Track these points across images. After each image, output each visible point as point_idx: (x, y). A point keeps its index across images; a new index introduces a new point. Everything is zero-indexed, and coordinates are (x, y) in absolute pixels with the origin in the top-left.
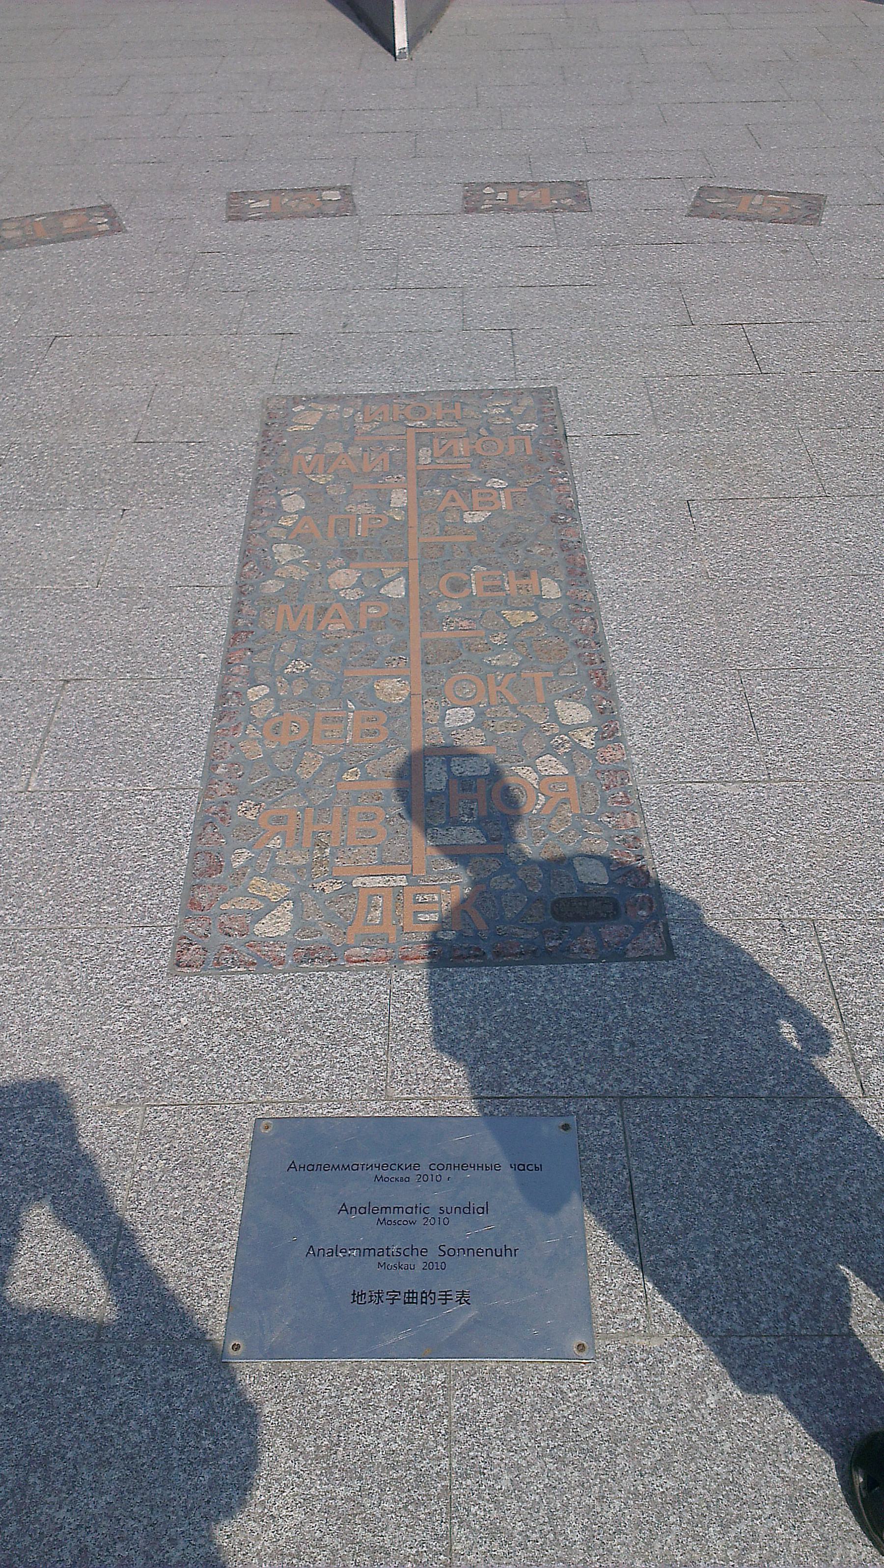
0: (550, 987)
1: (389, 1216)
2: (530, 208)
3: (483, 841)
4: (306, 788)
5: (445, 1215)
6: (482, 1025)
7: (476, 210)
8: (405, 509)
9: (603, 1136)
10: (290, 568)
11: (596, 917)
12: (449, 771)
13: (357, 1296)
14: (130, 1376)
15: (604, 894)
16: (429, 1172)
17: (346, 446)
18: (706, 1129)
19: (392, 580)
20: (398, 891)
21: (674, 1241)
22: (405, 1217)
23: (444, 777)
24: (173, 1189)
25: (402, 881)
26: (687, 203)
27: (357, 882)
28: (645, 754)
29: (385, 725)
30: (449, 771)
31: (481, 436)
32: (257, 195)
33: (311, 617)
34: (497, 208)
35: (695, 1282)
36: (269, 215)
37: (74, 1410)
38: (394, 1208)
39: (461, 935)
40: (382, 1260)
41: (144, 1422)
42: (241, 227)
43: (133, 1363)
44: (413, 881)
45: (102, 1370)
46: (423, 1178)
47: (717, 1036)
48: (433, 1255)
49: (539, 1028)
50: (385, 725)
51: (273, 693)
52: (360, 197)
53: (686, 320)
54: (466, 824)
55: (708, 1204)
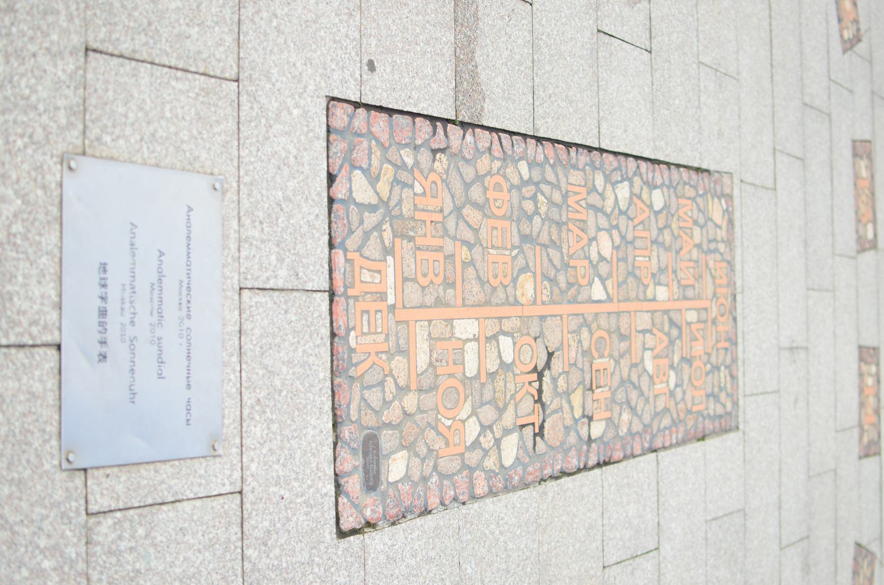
0: (317, 431)
1: (156, 292)
2: (862, 405)
3: (419, 371)
4: (458, 210)
5: (157, 342)
6: (291, 372)
7: (861, 359)
8: (654, 299)
9: (216, 476)
10: (612, 198)
11: (366, 471)
12: (468, 340)
13: (104, 268)
14: (64, 77)
15: (383, 478)
16: (185, 328)
17: (698, 246)
18: (221, 564)
19: (605, 288)
20: (383, 297)
21: (147, 536)
22: (156, 307)
23: (464, 337)
24: (183, 108)
25: (391, 300)
26: (864, 542)
27: (390, 259)
28: (480, 515)
29: (501, 283)
30: (468, 340)
31: (705, 365)
32: (871, 168)
33: (577, 216)
34: (861, 375)
35: (121, 552)
36: (857, 176)
37: (42, 32)
38: (377, 311)
39: (352, 350)
40: (128, 287)
41: (34, 91)
42: (848, 153)
43: (71, 78)
44: (392, 308)
45: (67, 54)
46: (181, 320)
47: (285, 575)
48: (130, 331)
49: (289, 422)
50: (501, 283)
51: (525, 183)
52: (869, 256)
53: (784, 543)
54: (431, 356)
55: (172, 565)
